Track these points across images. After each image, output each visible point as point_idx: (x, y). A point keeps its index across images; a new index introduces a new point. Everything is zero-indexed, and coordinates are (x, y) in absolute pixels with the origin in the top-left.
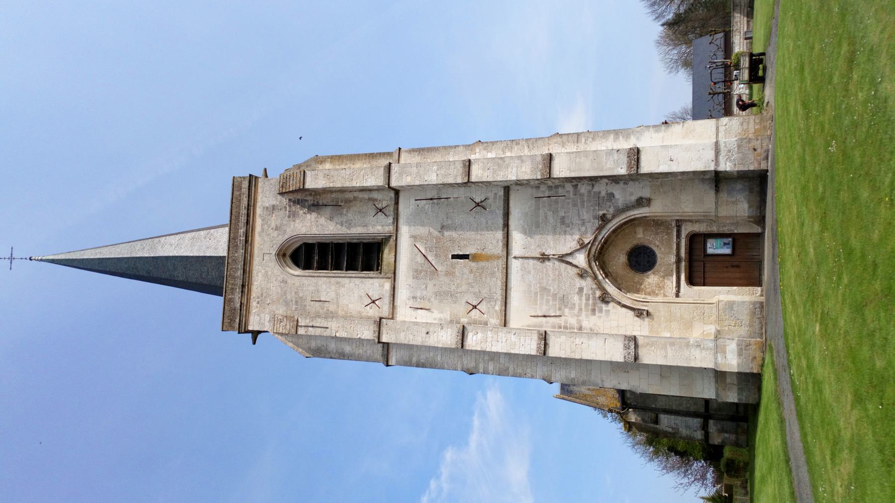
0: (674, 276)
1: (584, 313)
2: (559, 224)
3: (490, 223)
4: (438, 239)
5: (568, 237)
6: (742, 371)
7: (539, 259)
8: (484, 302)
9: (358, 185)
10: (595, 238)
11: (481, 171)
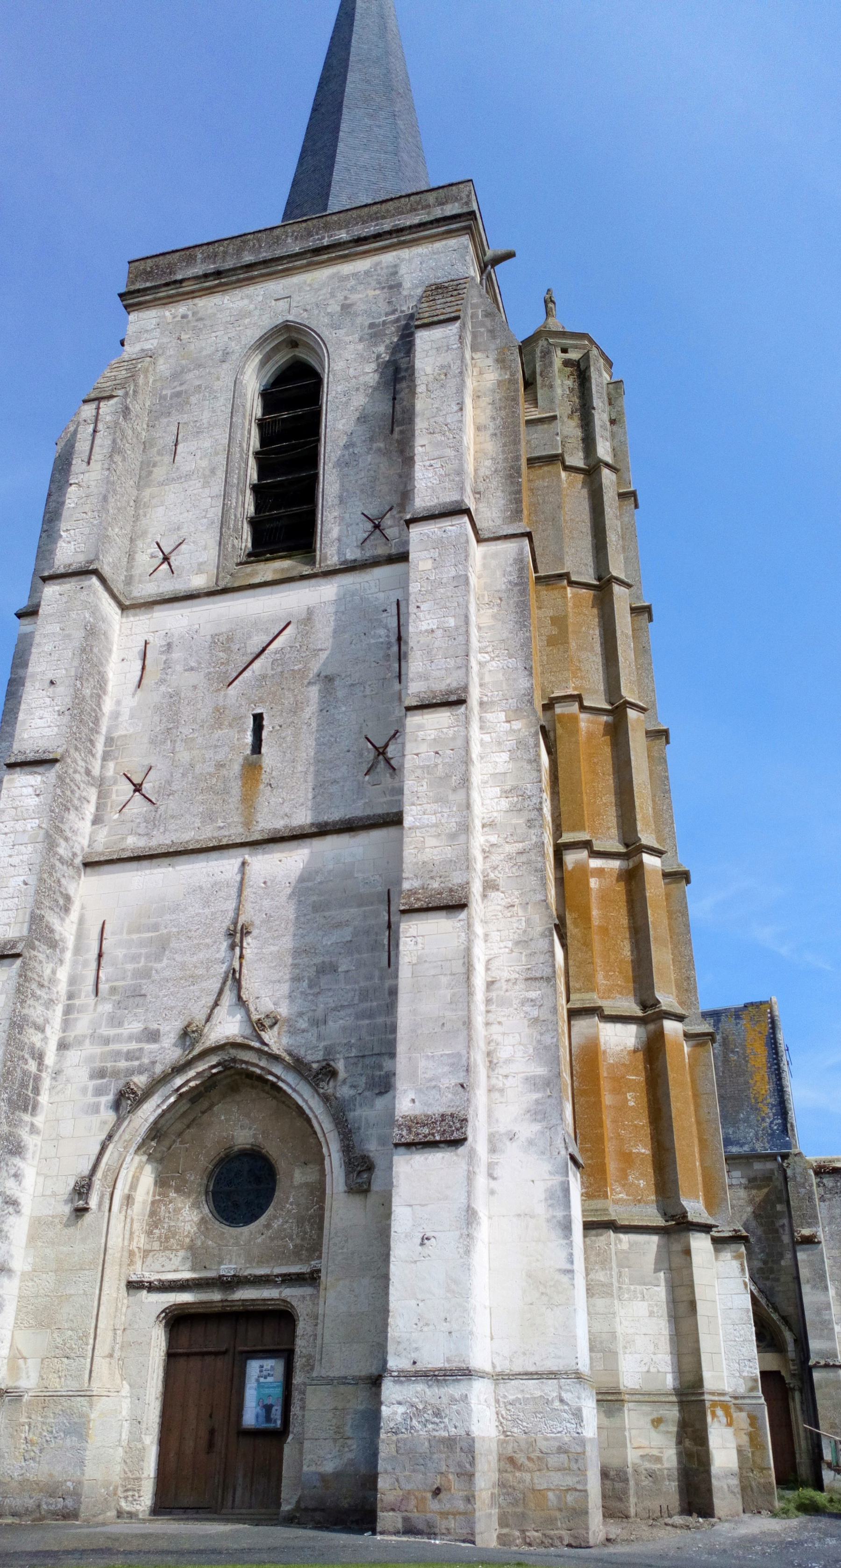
0: (187, 1275)
1: (98, 1050)
2: (318, 960)
3: (334, 789)
4: (303, 673)
5: (285, 988)
6: (477, 1445)
7: (235, 923)
8: (146, 807)
9: (418, 450)
10: (276, 1058)
11: (432, 734)
